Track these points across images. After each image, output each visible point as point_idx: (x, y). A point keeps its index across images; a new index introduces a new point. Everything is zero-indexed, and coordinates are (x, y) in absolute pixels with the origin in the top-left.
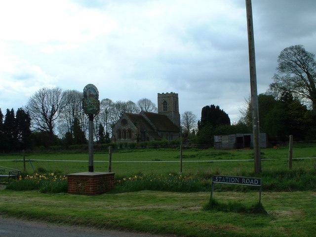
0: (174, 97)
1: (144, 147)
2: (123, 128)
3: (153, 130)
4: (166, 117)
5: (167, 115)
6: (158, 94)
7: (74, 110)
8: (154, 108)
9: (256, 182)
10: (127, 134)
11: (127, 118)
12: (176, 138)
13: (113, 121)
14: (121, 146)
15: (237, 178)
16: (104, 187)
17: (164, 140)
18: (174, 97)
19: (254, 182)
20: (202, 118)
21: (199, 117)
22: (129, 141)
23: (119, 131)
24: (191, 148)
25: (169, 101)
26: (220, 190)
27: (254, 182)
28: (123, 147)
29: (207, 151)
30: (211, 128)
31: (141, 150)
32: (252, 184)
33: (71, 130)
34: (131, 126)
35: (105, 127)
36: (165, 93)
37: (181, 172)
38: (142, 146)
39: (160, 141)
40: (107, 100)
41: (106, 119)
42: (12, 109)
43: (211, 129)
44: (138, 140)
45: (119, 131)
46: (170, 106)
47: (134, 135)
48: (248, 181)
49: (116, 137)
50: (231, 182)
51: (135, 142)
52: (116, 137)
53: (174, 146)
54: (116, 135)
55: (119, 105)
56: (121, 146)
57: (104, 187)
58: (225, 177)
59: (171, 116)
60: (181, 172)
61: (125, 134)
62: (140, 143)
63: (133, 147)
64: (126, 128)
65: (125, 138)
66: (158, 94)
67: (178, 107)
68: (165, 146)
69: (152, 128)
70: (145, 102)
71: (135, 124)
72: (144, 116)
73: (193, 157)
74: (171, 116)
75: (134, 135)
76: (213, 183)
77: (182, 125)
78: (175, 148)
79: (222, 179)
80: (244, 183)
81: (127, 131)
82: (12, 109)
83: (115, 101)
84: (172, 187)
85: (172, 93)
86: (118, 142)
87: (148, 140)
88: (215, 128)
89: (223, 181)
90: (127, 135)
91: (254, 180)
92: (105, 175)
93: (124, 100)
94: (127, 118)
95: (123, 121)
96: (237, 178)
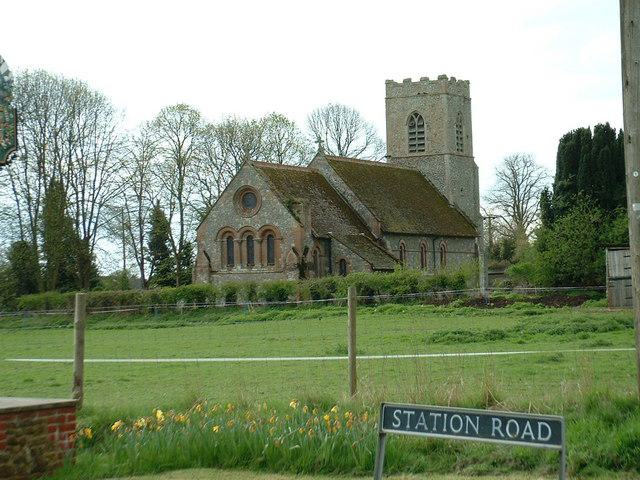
0: (455, 94)
1: (321, 297)
2: (241, 222)
3: (367, 230)
4: (420, 176)
5: (424, 168)
6: (390, 84)
7: (42, 147)
8: (371, 143)
9: (545, 434)
10: (257, 246)
11: (259, 183)
12: (458, 262)
13: (207, 195)
14: (231, 297)
15: (473, 416)
16: (29, 458)
17: (412, 269)
18: (455, 94)
19: (503, 429)
20: (559, 177)
21: (545, 170)
22: (265, 276)
23: (227, 237)
24: (511, 302)
25: (434, 111)
26: (483, 467)
27: (503, 429)
28: (240, 302)
29: (576, 313)
30: (594, 218)
31: (310, 312)
32: (528, 439)
33: (34, 230)
34: (273, 212)
35: (176, 218)
36: (415, 79)
37: (353, 390)
38: (316, 296)
39: (387, 276)
40: (182, 108)
41: (180, 190)
42: (607, 124)
43: (596, 224)
44: (303, 269)
45: (227, 237)
46: (438, 136)
47: (285, 251)
48: (513, 429)
49: (216, 260)
50: (449, 432)
51: (292, 277)
52: (216, 260)
53: (449, 292)
54: (215, 251)
55: (228, 133)
56: (231, 297)
57: (29, 458)
58: (427, 412)
59: (442, 174)
60: (353, 390)
61: (250, 248)
62: (313, 281)
63: (278, 298)
64: (255, 222)
65: (250, 262)
66: (390, 84)
67: (469, 137)
68: (409, 294)
69: (355, 219)
70: (337, 117)
71: (290, 206)
72: (328, 173)
73: (496, 336)
74: (440, 172)
75: (285, 251)
76: (382, 435)
77: (486, 208)
78: (446, 301)
79: (414, 419)
80: (498, 436)
81: (257, 237)
82: (607, 124)
83: (213, 115)
84: (296, 454)
85: (443, 78)
86: (220, 283)
87: (343, 272)
88: (614, 218)
89: (421, 429)
90: (236, 255)
91: (534, 423)
92: (40, 409)
93: (249, 110)
94: (259, 183)
95: (245, 197)
96: (473, 416)
